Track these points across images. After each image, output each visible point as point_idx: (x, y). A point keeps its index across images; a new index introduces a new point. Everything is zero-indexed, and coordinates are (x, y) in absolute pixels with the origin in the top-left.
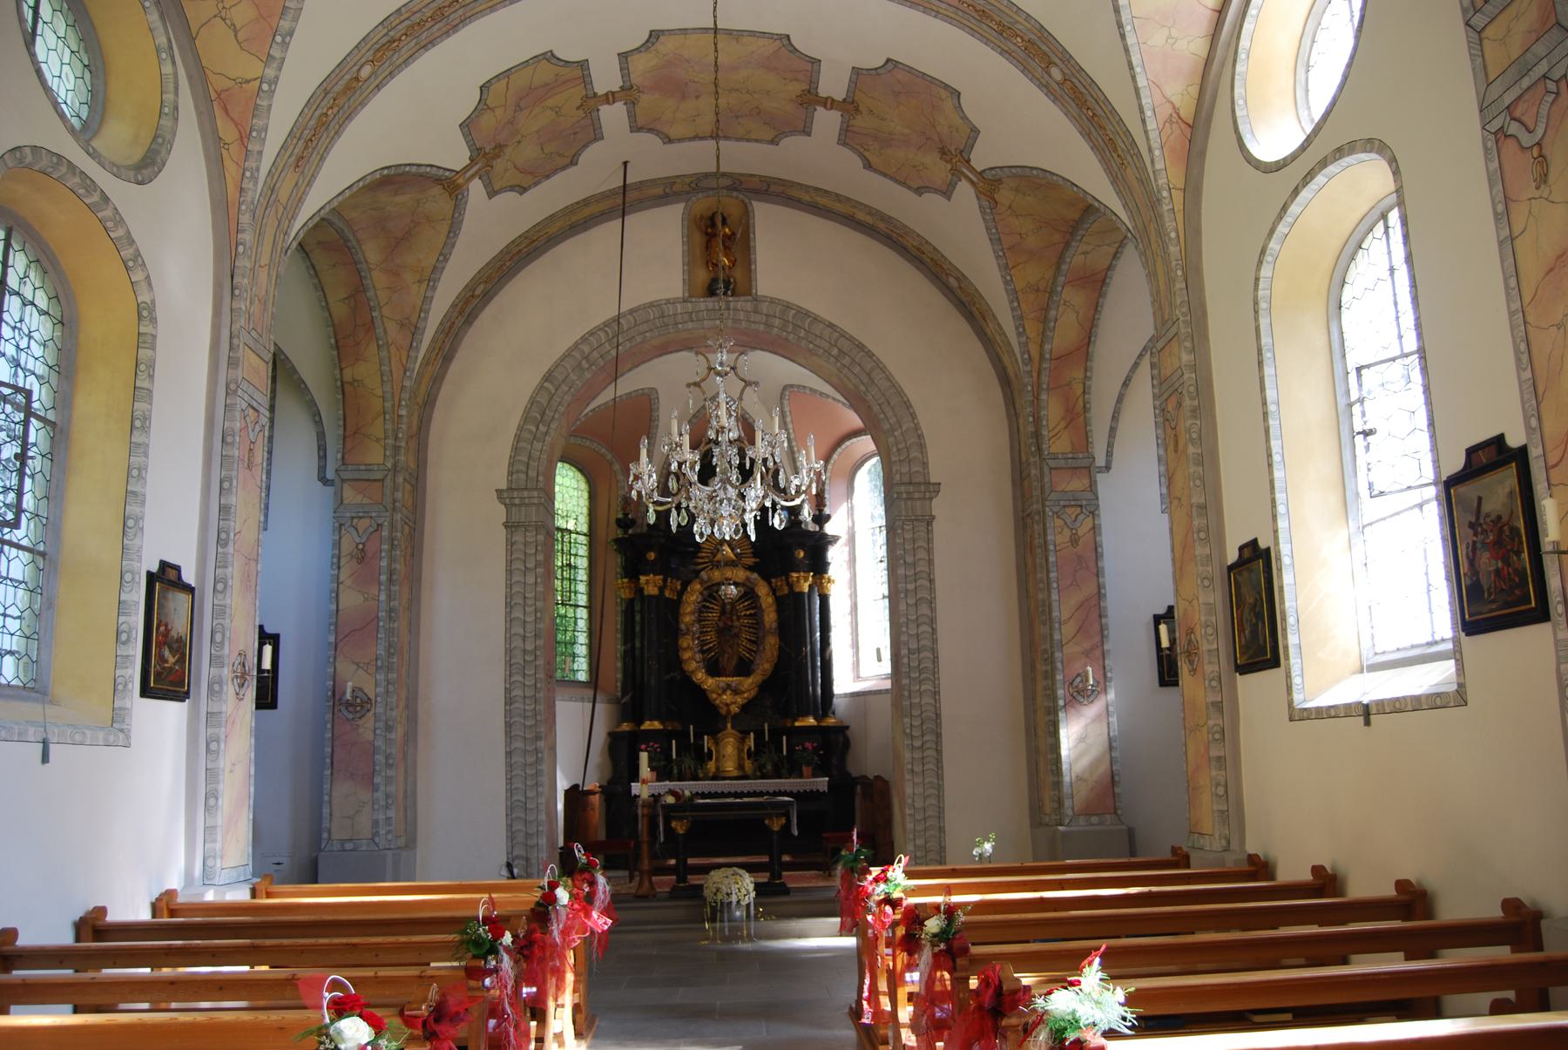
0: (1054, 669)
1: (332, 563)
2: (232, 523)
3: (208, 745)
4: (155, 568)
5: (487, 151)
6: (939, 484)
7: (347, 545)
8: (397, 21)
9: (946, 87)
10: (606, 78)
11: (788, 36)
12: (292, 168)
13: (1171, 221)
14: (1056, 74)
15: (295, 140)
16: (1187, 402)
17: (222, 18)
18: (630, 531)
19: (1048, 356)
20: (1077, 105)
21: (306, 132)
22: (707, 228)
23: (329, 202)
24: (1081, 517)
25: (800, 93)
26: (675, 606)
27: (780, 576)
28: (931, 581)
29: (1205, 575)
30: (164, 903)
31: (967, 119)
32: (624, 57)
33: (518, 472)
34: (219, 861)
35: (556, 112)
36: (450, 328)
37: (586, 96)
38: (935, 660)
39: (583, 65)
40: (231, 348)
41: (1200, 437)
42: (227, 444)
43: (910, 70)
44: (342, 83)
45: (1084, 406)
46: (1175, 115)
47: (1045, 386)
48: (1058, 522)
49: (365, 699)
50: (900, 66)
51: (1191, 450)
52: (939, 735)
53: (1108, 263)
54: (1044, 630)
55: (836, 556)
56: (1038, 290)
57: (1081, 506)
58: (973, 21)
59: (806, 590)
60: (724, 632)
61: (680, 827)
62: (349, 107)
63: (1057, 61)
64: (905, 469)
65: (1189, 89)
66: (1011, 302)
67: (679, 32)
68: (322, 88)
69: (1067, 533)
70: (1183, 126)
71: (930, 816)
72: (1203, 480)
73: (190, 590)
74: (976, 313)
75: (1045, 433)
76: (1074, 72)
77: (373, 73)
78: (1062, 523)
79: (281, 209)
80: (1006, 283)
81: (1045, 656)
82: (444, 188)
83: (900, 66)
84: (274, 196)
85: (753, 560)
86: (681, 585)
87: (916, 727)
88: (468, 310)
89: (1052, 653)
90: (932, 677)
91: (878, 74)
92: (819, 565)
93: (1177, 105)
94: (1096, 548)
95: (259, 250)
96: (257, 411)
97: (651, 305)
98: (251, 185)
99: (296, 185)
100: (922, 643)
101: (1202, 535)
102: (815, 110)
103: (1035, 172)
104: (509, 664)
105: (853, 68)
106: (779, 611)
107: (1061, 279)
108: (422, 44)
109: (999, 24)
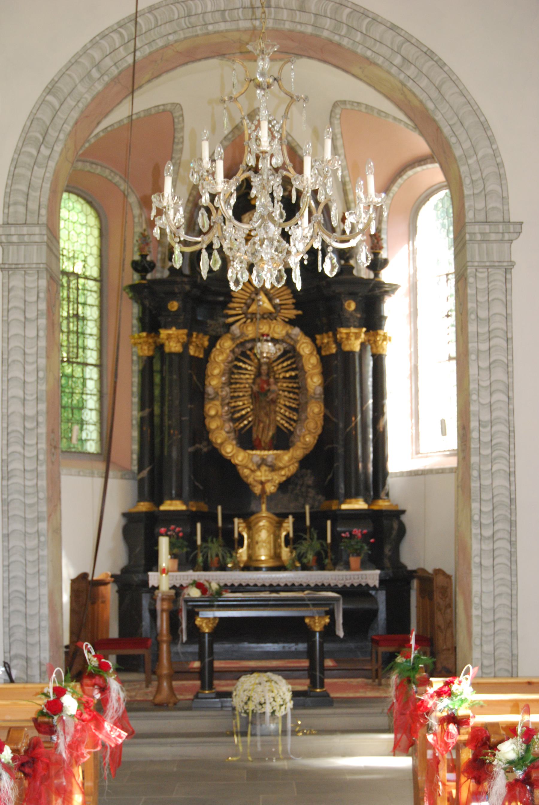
6: (521, 223)
18: (149, 276)
27: (327, 332)
33: (15, 204)
38: (511, 434)
52: (513, 524)
71: (499, 619)
87: (486, 513)
100: (495, 414)
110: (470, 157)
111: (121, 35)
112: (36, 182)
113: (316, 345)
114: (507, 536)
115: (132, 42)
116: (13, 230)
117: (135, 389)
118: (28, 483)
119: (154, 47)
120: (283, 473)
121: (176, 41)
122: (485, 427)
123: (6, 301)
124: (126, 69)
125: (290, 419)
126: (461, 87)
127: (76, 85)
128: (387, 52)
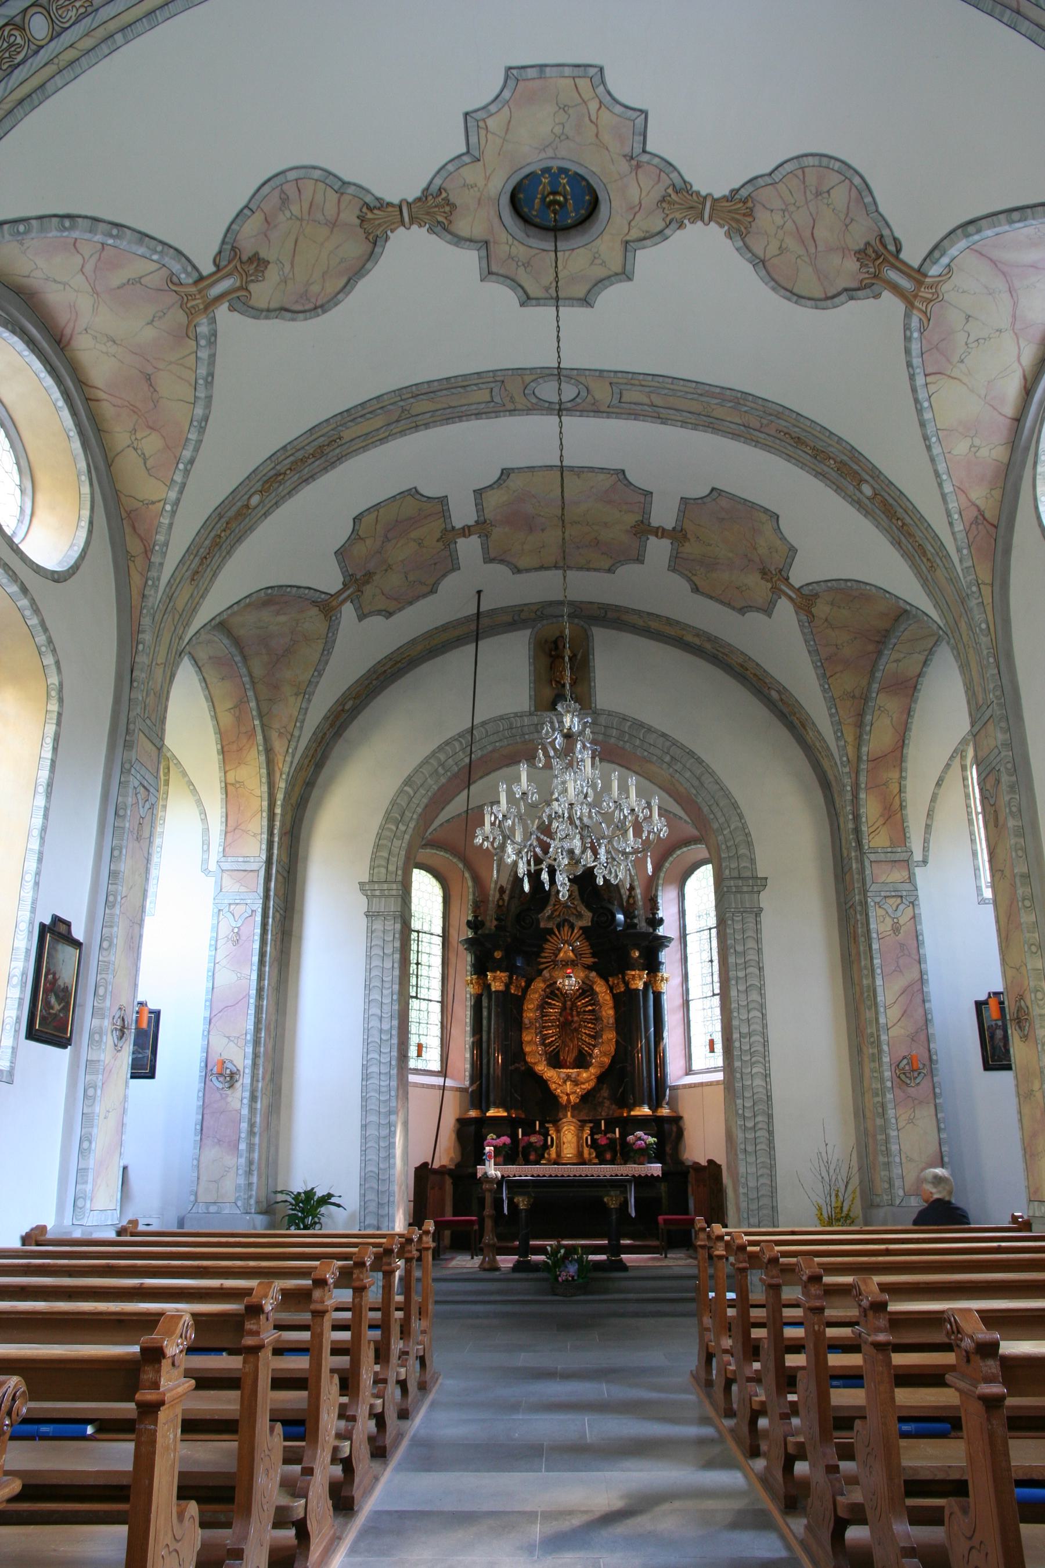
0: (880, 1051)
1: (211, 945)
2: (120, 888)
3: (85, 1091)
4: (47, 921)
5: (358, 577)
6: (766, 878)
7: (224, 931)
8: (283, 457)
9: (766, 511)
10: (463, 513)
11: (623, 471)
12: (189, 580)
13: (980, 614)
14: (867, 490)
15: (192, 557)
16: (1005, 779)
17: (134, 448)
18: (480, 932)
19: (865, 758)
20: (887, 517)
21: (202, 550)
22: (551, 650)
23: (219, 614)
24: (902, 907)
25: (634, 523)
26: (518, 1002)
27: (617, 975)
28: (761, 969)
29: (1031, 941)
30: (34, 1237)
31: (786, 539)
32: (479, 493)
33: (379, 866)
34: (88, 1203)
35: (419, 544)
36: (322, 738)
37: (445, 529)
38: (765, 1043)
39: (443, 501)
40: (127, 732)
41: (1020, 811)
42: (119, 816)
43: (732, 497)
44: (235, 509)
45: (901, 805)
46: (980, 517)
47: (863, 786)
48: (881, 912)
49: (235, 1070)
50: (724, 494)
51: (1011, 823)
52: (770, 1117)
53: (918, 670)
54: (869, 1015)
55: (668, 957)
56: (854, 697)
57: (901, 897)
58: (789, 448)
59: (641, 986)
60: (566, 1027)
61: (522, 1202)
62: (240, 531)
63: (867, 478)
64: (734, 865)
65: (993, 492)
66: (829, 709)
67: (526, 470)
68: (217, 512)
69: (889, 921)
70: (989, 527)
71: (763, 1196)
72: (1024, 850)
73: (77, 944)
74: (796, 722)
75: (864, 828)
76: (884, 486)
77: (261, 502)
78: (884, 913)
79: (177, 617)
80: (824, 691)
81: (872, 1040)
82: (320, 610)
83: (724, 494)
84: (171, 605)
85: (593, 960)
86: (525, 982)
87: (748, 1108)
88: (338, 724)
89: (879, 1036)
90: (762, 1060)
91: (704, 503)
92: (653, 966)
93: (982, 508)
94: (917, 937)
95: (157, 648)
96: (148, 791)
97: (501, 718)
98: (152, 592)
99: (192, 595)
100: (752, 1028)
101: (1027, 903)
102: (648, 539)
103: (849, 584)
104: (367, 1043)
105: (682, 498)
106: (616, 1007)
107: (875, 686)
108: (304, 478)
109: (814, 449)
110: (725, 829)
111: (461, 743)
112: (395, 850)
113: (609, 985)
114: (766, 1127)
115: (469, 748)
116: (376, 887)
117: (468, 1020)
118: (382, 1083)
119: (485, 752)
120: (583, 1086)
121: (501, 747)
122: (745, 1038)
123: (369, 940)
124: (463, 767)
125: (589, 1044)
126: (716, 778)
127: (427, 779)
128: (659, 753)
